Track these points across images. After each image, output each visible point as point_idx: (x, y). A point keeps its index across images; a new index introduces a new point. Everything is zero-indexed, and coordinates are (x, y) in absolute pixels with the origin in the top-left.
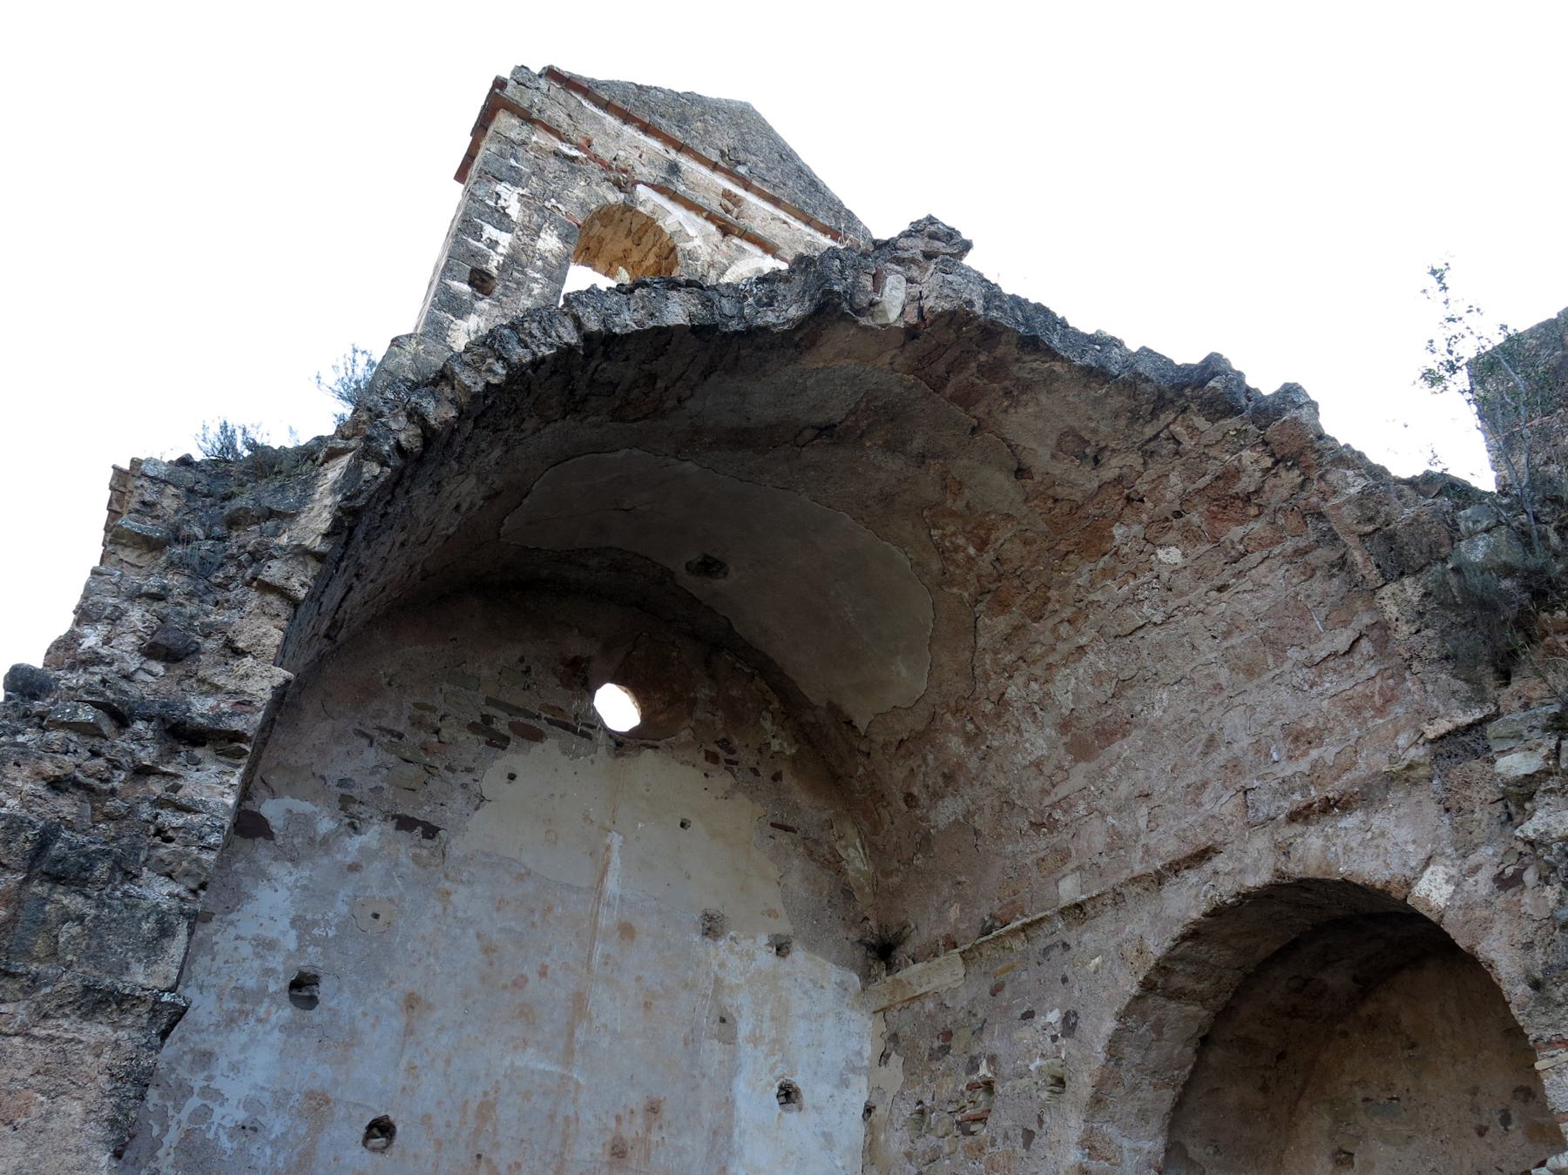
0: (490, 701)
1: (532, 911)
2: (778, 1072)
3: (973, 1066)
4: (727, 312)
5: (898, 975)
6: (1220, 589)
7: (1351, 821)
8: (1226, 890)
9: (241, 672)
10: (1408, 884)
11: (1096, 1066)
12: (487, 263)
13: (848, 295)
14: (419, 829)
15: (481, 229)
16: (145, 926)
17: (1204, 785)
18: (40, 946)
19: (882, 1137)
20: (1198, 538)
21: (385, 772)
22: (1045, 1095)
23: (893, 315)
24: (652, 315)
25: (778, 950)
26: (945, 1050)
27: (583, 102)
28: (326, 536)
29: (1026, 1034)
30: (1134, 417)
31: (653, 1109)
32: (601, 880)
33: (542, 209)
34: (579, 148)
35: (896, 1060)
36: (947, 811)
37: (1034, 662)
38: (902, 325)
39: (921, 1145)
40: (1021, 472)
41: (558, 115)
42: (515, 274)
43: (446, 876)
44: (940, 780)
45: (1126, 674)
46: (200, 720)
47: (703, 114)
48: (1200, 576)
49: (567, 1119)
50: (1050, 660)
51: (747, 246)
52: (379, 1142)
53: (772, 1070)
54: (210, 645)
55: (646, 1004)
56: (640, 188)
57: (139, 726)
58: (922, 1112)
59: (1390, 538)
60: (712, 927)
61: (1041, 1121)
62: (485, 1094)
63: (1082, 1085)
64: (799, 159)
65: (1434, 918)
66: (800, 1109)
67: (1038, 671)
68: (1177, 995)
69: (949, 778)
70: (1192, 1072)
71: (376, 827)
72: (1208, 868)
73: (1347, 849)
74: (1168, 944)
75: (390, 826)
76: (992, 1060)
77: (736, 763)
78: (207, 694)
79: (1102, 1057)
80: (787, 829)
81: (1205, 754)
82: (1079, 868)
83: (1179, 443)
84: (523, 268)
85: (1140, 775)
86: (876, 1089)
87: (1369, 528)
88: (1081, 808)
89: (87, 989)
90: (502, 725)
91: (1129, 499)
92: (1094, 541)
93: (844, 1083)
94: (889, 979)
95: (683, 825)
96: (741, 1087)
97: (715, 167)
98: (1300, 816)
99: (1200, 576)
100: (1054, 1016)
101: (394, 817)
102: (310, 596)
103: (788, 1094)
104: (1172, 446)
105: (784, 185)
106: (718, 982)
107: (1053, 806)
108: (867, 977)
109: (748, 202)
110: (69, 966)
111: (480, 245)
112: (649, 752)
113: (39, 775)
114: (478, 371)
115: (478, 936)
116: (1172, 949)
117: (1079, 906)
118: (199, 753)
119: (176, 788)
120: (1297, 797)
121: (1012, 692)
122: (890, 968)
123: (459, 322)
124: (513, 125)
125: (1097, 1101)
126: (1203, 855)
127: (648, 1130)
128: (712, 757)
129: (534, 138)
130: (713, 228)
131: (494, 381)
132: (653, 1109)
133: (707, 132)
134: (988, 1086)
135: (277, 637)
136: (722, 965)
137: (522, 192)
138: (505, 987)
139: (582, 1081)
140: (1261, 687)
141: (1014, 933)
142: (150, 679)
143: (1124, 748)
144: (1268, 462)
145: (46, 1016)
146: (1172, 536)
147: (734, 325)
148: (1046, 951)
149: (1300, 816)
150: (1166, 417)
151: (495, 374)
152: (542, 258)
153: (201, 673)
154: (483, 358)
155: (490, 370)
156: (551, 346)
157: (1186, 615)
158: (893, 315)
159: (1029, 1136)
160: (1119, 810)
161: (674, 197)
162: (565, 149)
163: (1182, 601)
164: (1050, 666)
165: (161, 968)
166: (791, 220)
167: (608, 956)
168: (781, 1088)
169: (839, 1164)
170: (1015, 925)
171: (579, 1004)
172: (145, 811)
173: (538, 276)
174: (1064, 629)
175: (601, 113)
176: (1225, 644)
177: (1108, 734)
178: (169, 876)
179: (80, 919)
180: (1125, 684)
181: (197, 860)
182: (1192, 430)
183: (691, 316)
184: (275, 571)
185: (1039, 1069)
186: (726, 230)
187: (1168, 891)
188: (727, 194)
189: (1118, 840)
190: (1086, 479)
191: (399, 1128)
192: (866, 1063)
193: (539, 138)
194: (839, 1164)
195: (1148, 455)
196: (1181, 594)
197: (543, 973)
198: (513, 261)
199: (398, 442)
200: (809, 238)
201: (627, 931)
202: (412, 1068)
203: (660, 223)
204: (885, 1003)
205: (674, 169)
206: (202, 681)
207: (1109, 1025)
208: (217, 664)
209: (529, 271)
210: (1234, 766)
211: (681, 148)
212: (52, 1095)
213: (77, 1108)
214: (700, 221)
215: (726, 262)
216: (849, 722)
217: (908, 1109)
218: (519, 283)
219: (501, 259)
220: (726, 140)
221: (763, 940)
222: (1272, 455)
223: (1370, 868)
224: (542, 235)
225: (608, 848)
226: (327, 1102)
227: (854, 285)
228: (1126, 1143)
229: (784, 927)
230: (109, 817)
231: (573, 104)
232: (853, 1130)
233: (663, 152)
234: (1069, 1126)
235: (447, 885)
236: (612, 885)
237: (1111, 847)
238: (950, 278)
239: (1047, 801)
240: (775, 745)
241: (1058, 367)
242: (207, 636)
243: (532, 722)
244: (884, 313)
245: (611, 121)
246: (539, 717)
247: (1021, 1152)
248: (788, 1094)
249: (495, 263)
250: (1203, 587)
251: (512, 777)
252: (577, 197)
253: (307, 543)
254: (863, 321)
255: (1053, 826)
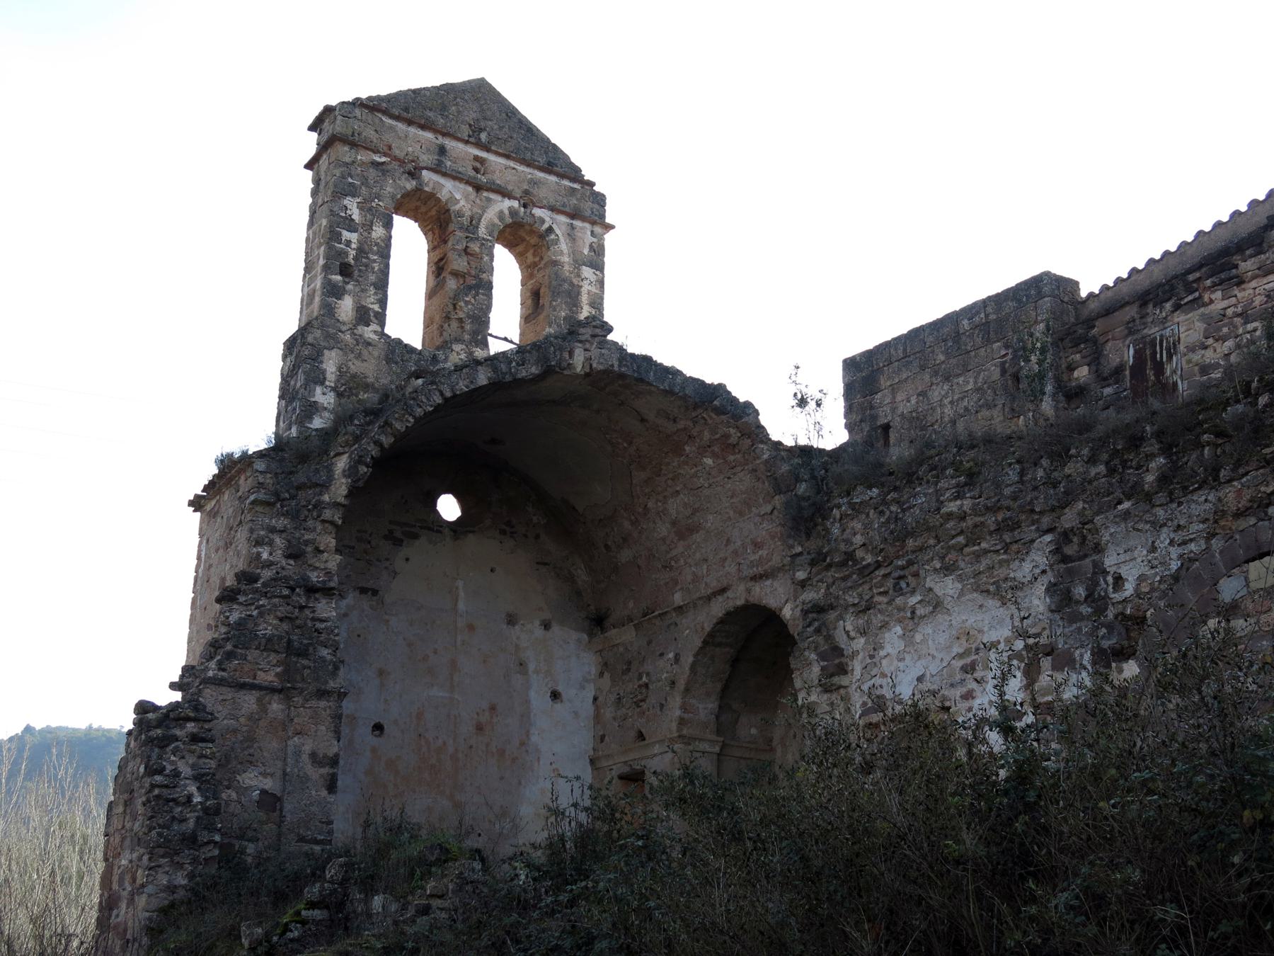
0: (391, 522)
1: (426, 624)
2: (549, 686)
3: (640, 678)
4: (504, 370)
5: (606, 635)
6: (729, 478)
7: (768, 582)
8: (730, 605)
9: (324, 560)
10: (781, 610)
11: (686, 676)
12: (347, 257)
13: (559, 364)
14: (370, 592)
15: (340, 234)
16: (330, 667)
17: (726, 559)
18: (298, 678)
19: (602, 711)
20: (718, 457)
21: (349, 567)
22: (668, 688)
23: (579, 369)
24: (472, 382)
25: (545, 626)
26: (628, 670)
27: (383, 119)
28: (346, 497)
29: (661, 663)
30: (687, 408)
31: (493, 708)
32: (456, 605)
33: (370, 209)
34: (385, 155)
35: (607, 675)
36: (625, 555)
37: (659, 494)
38: (582, 373)
39: (619, 713)
40: (643, 420)
41: (369, 133)
42: (364, 260)
43: (386, 613)
44: (621, 540)
45: (696, 506)
46: (319, 585)
47: (455, 98)
48: (720, 472)
49: (455, 716)
50: (665, 494)
51: (492, 196)
52: (377, 733)
53: (546, 685)
54: (309, 549)
55: (484, 661)
56: (424, 173)
57: (298, 590)
58: (619, 698)
59: (776, 479)
60: (511, 620)
61: (666, 700)
62: (419, 708)
63: (681, 685)
64: (519, 113)
65: (786, 622)
66: (562, 701)
67: (660, 498)
68: (720, 645)
69: (625, 540)
70: (729, 675)
71: (351, 595)
72: (725, 595)
73: (766, 594)
74: (712, 626)
75: (357, 593)
76: (648, 674)
77: (516, 533)
78: (313, 570)
79: (688, 672)
80: (545, 564)
81: (726, 545)
82: (682, 589)
83: (706, 420)
84: (367, 254)
85: (704, 551)
86: (599, 689)
87: (769, 474)
88: (682, 562)
89: (318, 690)
90: (398, 534)
91: (690, 436)
92: (678, 450)
93: (583, 688)
94: (602, 636)
95: (492, 571)
96: (532, 694)
97: (467, 142)
98: (754, 578)
99: (720, 472)
100: (671, 655)
101: (358, 588)
102: (343, 522)
103: (555, 696)
104: (703, 421)
105: (511, 138)
106: (517, 646)
107: (671, 559)
108: (591, 635)
109: (490, 160)
110: (310, 683)
111: (342, 246)
112: (471, 535)
113: (277, 617)
114: (402, 421)
115: (404, 639)
116: (713, 628)
117: (680, 607)
118: (317, 595)
119: (314, 612)
120: (755, 569)
121: (650, 505)
122: (603, 630)
123: (339, 302)
124: (346, 152)
125: (687, 690)
126: (723, 591)
127: (492, 717)
128: (503, 532)
129: (359, 157)
130: (470, 189)
131: (409, 425)
132: (493, 708)
133: (459, 112)
134: (646, 685)
135: (333, 542)
136: (518, 638)
137: (358, 200)
138: (420, 661)
139: (460, 699)
140: (744, 521)
141: (655, 617)
142: (290, 567)
143: (698, 537)
144: (739, 435)
145: (307, 701)
146: (707, 454)
147: (508, 378)
148: (668, 626)
149: (754, 578)
150: (700, 411)
151: (409, 422)
152: (377, 244)
153: (309, 562)
154: (404, 415)
155: (407, 421)
156: (431, 406)
157: (717, 486)
158: (579, 369)
159: (662, 706)
160: (696, 565)
161: (444, 175)
162: (378, 158)
163: (715, 480)
164: (665, 497)
165: (338, 680)
166: (521, 168)
167: (463, 641)
168: (552, 693)
169: (582, 724)
170: (656, 613)
171: (453, 665)
172: (310, 624)
173: (376, 257)
174: (670, 482)
175: (394, 123)
176: (732, 501)
177: (692, 529)
178: (325, 647)
179: (310, 667)
180: (695, 511)
181: (335, 640)
182: (711, 418)
183: (489, 379)
184: (327, 514)
185: (665, 678)
186: (478, 188)
187: (713, 603)
188: (476, 158)
189: (696, 579)
190: (671, 427)
191: (385, 727)
192: (593, 677)
193: (362, 156)
194: (582, 724)
195: (695, 423)
196: (714, 477)
197: (435, 652)
198: (361, 251)
199: (372, 456)
200: (529, 176)
201: (471, 628)
202: (386, 701)
203: (439, 195)
204: (600, 647)
205: (442, 150)
206: (310, 566)
207: (691, 659)
208: (313, 557)
209: (371, 256)
210: (735, 552)
211: (444, 135)
212: (316, 724)
213: (323, 728)
214: (462, 186)
215: (480, 211)
216: (574, 508)
217: (613, 697)
218: (366, 266)
219: (354, 252)
220: (471, 115)
221: (537, 623)
222: (740, 432)
223: (771, 602)
224: (374, 228)
225: (457, 588)
226: (355, 718)
227: (560, 359)
228: (701, 706)
229: (547, 615)
230: (298, 627)
231: (377, 121)
232: (588, 708)
233: (434, 140)
234: (676, 701)
235: (387, 617)
236: (461, 606)
237: (693, 581)
238: (603, 351)
239: (669, 556)
240: (535, 519)
241: (653, 388)
242: (306, 545)
243: (412, 530)
244: (575, 368)
245: (401, 126)
246: (415, 526)
247: (659, 713)
248: (555, 696)
249: (352, 256)
250: (722, 477)
251: (407, 560)
252: (389, 193)
253: (338, 500)
254: (565, 372)
255: (671, 568)
